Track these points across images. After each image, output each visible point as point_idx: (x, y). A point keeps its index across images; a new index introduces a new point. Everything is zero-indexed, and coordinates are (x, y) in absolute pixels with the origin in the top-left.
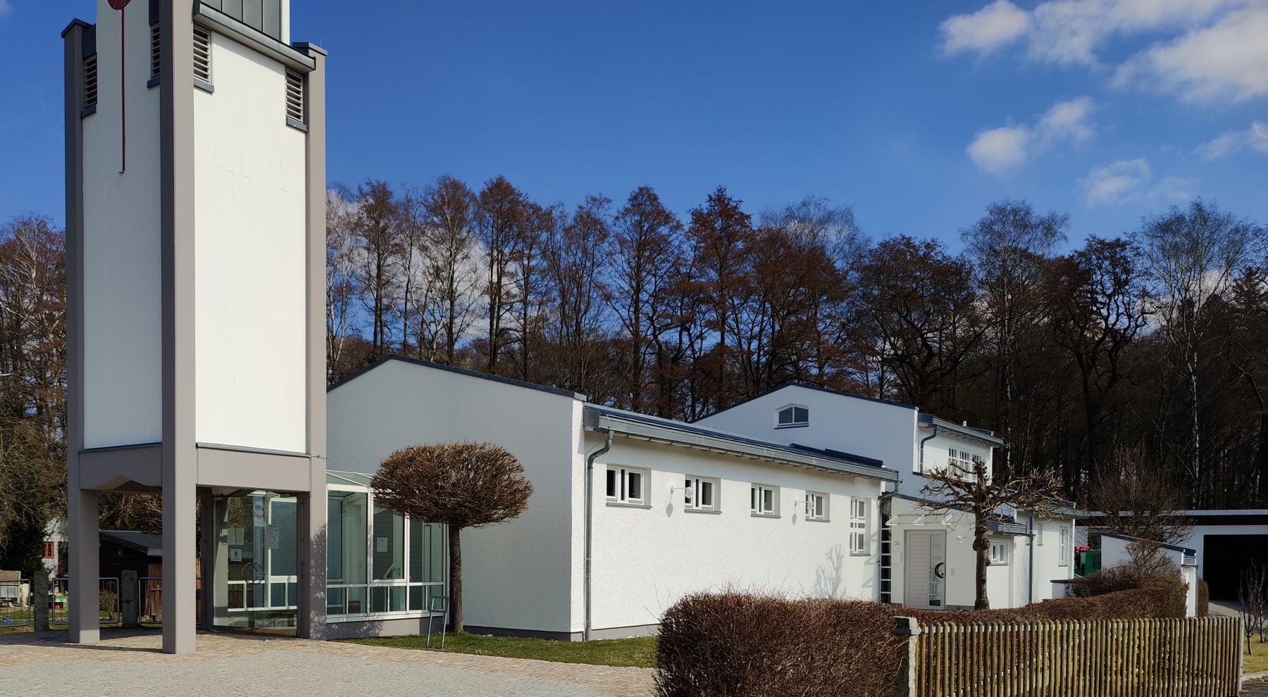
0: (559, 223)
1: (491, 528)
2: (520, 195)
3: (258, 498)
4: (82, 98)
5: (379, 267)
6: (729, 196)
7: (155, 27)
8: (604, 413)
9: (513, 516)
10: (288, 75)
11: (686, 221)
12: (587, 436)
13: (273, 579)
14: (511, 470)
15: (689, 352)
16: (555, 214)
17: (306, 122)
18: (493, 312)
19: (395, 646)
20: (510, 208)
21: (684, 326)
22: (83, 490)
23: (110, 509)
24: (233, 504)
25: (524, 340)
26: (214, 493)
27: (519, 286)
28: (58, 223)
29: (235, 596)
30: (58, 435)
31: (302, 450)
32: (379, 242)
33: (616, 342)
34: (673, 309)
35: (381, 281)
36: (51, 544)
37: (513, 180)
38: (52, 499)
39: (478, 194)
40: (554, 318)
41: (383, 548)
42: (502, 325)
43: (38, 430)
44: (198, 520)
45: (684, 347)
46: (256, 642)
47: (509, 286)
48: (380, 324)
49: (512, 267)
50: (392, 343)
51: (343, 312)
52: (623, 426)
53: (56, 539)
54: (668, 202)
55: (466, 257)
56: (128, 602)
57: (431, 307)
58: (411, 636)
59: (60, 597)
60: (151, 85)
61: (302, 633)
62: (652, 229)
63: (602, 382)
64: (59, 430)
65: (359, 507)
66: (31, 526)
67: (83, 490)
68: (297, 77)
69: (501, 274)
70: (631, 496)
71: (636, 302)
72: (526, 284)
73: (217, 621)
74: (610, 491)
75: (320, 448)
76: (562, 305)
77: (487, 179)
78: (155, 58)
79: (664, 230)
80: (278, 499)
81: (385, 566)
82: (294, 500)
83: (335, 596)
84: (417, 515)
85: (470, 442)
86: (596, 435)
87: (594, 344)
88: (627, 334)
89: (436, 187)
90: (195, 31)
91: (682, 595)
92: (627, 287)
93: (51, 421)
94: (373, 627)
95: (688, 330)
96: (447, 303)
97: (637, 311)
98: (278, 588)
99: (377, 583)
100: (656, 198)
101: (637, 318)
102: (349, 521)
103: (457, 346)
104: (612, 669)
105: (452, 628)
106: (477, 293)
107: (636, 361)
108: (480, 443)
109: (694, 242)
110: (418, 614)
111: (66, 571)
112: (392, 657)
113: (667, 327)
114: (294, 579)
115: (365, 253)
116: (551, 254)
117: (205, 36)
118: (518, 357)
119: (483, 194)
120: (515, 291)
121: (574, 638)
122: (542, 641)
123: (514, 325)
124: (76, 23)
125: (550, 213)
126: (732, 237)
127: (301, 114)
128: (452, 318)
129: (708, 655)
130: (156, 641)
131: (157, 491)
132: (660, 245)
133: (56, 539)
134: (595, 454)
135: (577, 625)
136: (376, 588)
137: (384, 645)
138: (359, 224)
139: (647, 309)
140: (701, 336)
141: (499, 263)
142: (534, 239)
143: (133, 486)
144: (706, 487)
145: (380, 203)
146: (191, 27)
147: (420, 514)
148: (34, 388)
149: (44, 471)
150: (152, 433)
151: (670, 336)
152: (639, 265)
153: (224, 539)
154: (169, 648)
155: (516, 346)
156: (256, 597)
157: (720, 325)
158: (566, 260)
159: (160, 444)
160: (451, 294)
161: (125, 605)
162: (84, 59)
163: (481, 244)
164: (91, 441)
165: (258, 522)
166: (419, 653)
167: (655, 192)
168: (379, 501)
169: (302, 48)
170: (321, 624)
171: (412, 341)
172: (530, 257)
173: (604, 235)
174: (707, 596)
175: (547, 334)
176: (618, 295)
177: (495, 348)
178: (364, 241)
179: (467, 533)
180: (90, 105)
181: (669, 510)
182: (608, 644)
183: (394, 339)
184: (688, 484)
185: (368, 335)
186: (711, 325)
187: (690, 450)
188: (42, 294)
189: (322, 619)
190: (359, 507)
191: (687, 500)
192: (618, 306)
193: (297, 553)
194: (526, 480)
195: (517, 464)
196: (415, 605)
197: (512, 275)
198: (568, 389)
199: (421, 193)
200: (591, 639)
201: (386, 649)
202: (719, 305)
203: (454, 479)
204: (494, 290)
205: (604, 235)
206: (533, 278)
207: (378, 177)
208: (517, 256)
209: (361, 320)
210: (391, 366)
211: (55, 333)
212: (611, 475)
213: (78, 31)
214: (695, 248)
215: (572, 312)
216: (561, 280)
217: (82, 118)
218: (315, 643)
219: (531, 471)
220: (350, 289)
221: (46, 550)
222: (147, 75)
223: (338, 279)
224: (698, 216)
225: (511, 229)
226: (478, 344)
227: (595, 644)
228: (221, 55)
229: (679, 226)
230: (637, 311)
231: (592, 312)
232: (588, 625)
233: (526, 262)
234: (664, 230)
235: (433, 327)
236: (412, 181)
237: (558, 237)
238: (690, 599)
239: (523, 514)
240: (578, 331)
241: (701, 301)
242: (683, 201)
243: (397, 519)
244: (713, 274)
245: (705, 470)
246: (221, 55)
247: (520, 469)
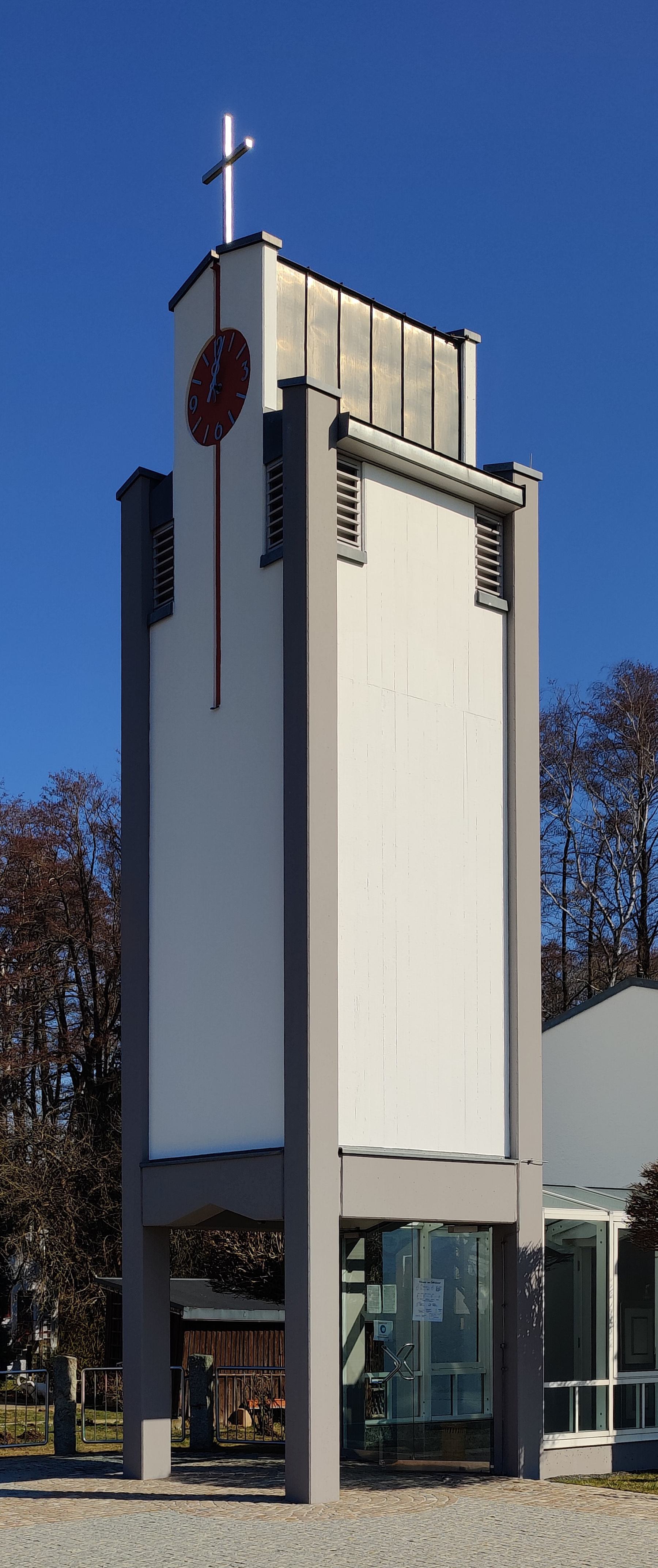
4: (149, 593)
7: (272, 467)
10: (479, 521)
31: (499, 1150)
60: (266, 562)
68: (496, 520)
89: (611, 684)
130: (268, 1477)
150: (270, 1131)
159: (281, 1150)
169: (504, 473)
217: (149, 627)
222: (258, 546)
246: (377, 496)
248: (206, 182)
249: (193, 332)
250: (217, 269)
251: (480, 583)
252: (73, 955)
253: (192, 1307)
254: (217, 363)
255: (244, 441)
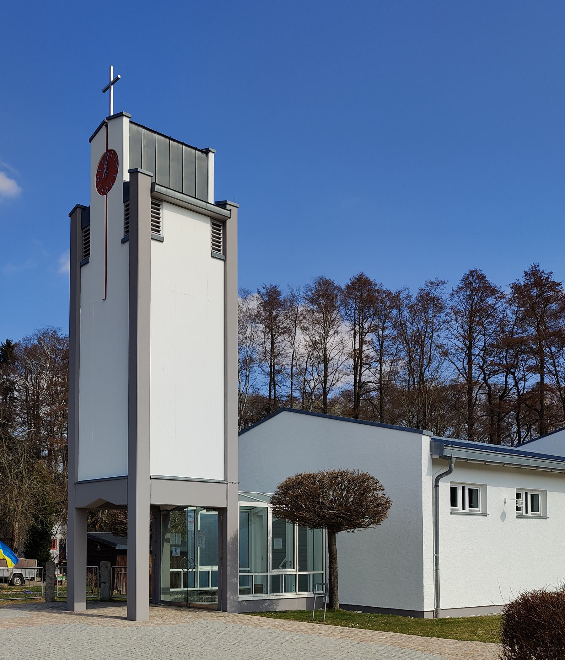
0: (406, 302)
1: (359, 532)
2: (376, 285)
3: (191, 511)
4: (81, 255)
5: (272, 344)
6: (541, 270)
7: (127, 203)
8: (448, 443)
9: (377, 523)
11: (508, 292)
12: (434, 462)
13: (201, 568)
14: (375, 489)
15: (514, 391)
16: (402, 296)
17: (225, 253)
18: (356, 370)
19: (288, 619)
20: (368, 295)
21: (509, 370)
22: (76, 508)
23: (92, 517)
24: (175, 517)
25: (380, 389)
26: (161, 509)
27: (376, 351)
28: (64, 332)
29: (175, 580)
30: (61, 468)
31: (222, 478)
32: (272, 325)
33: (454, 387)
34: (500, 359)
35: (274, 353)
36: (55, 541)
37: (371, 275)
38: (57, 511)
39: (343, 287)
40: (403, 373)
41: (278, 546)
42: (363, 380)
43: (49, 466)
44: (151, 526)
45: (510, 387)
46: (190, 613)
47: (368, 351)
48: (273, 383)
49: (369, 337)
50: (282, 396)
51: (247, 376)
52: (462, 454)
53: (59, 537)
54: (493, 279)
55: (336, 332)
56: (104, 583)
57: (310, 369)
58: (300, 611)
59: (60, 577)
60: (123, 241)
61: (222, 607)
62: (481, 300)
63: (442, 417)
64: (61, 465)
65: (261, 517)
66: (43, 529)
67: (76, 508)
68: (219, 224)
69: (362, 343)
70: (470, 506)
71: (470, 355)
72: (381, 349)
73: (162, 598)
74: (454, 502)
75: (234, 477)
76: (410, 362)
77: (351, 276)
78: (127, 223)
79: (490, 300)
80: (204, 512)
81: (280, 559)
82: (216, 513)
83: (244, 581)
84: (303, 523)
85: (343, 469)
86: (440, 459)
87: (436, 389)
88: (462, 380)
89: (313, 285)
90: (152, 203)
91: (522, 592)
92: (461, 345)
93: (56, 460)
94: (272, 604)
95: (513, 374)
96: (322, 366)
97: (470, 362)
98: (204, 574)
99: (276, 572)
100: (484, 277)
101: (470, 368)
102: (255, 527)
103: (329, 396)
104: (459, 644)
105: (331, 605)
106: (343, 358)
107: (470, 400)
108: (351, 470)
109: (515, 308)
110: (305, 594)
111: (64, 558)
112: (287, 628)
113: (495, 373)
114: (216, 568)
115: (262, 335)
116: (399, 325)
117: (159, 205)
118: (376, 402)
119: (348, 287)
120: (373, 354)
121: (426, 616)
122: (401, 617)
123: (372, 379)
124: (78, 206)
125: (399, 296)
126: (547, 301)
127: (221, 248)
128: (326, 376)
129: (547, 641)
130: (122, 611)
131: (124, 508)
132: (487, 312)
133: (59, 537)
134: (441, 476)
135: (428, 605)
136: (273, 577)
137: (280, 618)
138: (258, 315)
139: (478, 360)
140: (524, 379)
141: (361, 335)
142: (387, 316)
143: (108, 505)
144: (534, 498)
145: (272, 300)
146: (150, 200)
147: (306, 522)
148: (46, 439)
149: (52, 493)
150: (122, 470)
151: (498, 380)
152: (471, 328)
153: (168, 540)
154: (131, 617)
155: (373, 394)
156: (189, 580)
157: (539, 369)
158: (411, 329)
160: (326, 360)
161: (102, 585)
162: (82, 229)
163: (348, 323)
164: (82, 477)
165: (190, 527)
166: (307, 625)
167: (483, 272)
168: (275, 513)
169: (222, 204)
170: (235, 601)
171: (296, 394)
172: (383, 329)
173: (440, 308)
174: (545, 593)
175: (398, 384)
176: (454, 351)
177: (358, 396)
178: (261, 327)
179: (341, 536)
180: (85, 261)
181: (503, 516)
182: (455, 622)
183: (283, 393)
184: (518, 496)
185: (265, 392)
186: (531, 369)
187: (520, 470)
188: (53, 377)
189: (235, 598)
190: (261, 517)
191: (518, 509)
192: (454, 360)
193: (218, 552)
194: (386, 496)
195: (379, 484)
196: (303, 588)
197: (371, 342)
198: (418, 428)
199: (302, 290)
200: (440, 616)
201: (282, 621)
202: (539, 353)
203: (331, 497)
204: (357, 355)
205: (440, 308)
206: (386, 344)
207: (271, 282)
208: (374, 329)
209: (260, 383)
210: (284, 416)
211: (60, 403)
212: (453, 491)
213: (79, 211)
214: (515, 313)
215: (416, 368)
216: (408, 344)
217: (81, 267)
218: (231, 615)
219: (390, 488)
220: (252, 360)
221: (51, 544)
223: (244, 353)
224: (517, 288)
225: (369, 310)
226: (345, 394)
227: (444, 621)
228: (168, 215)
229: (502, 296)
230: (470, 362)
231: (434, 365)
232: (438, 606)
233: (380, 332)
234: (490, 300)
235: (312, 383)
236: (295, 282)
237: (405, 312)
238: (529, 595)
239: (385, 521)
240: (422, 381)
241: (523, 352)
242: (505, 276)
243: (289, 526)
244: (532, 330)
245: (532, 484)
246: (168, 215)
247: (381, 488)
248: (104, 92)
249: (97, 151)
250: (107, 126)
251: (213, 248)
252: (15, 402)
253: (121, 544)
254: (106, 163)
255: (116, 192)
